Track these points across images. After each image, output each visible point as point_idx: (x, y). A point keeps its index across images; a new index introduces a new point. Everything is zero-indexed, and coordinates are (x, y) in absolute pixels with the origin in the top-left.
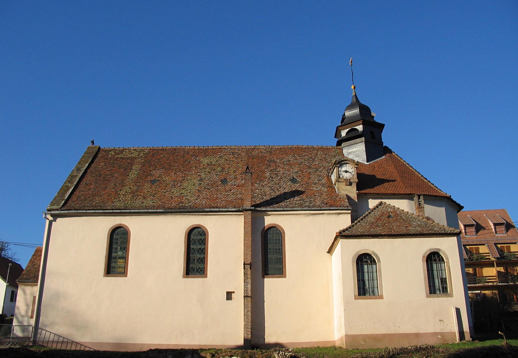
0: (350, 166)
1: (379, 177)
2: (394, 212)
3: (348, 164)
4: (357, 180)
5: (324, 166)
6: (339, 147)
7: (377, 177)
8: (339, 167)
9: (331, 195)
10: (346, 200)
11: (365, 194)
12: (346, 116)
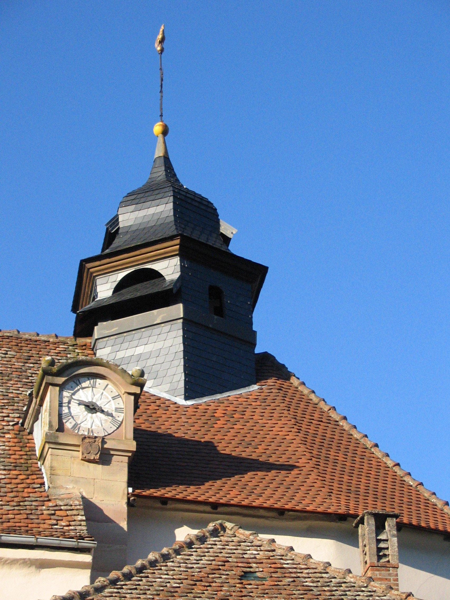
0: (111, 386)
1: (227, 451)
2: (269, 561)
3: (102, 377)
4: (135, 443)
5: (11, 395)
6: (81, 341)
7: (218, 448)
8: (62, 387)
9: (20, 494)
10: (80, 518)
11: (164, 501)
12: (121, 225)
